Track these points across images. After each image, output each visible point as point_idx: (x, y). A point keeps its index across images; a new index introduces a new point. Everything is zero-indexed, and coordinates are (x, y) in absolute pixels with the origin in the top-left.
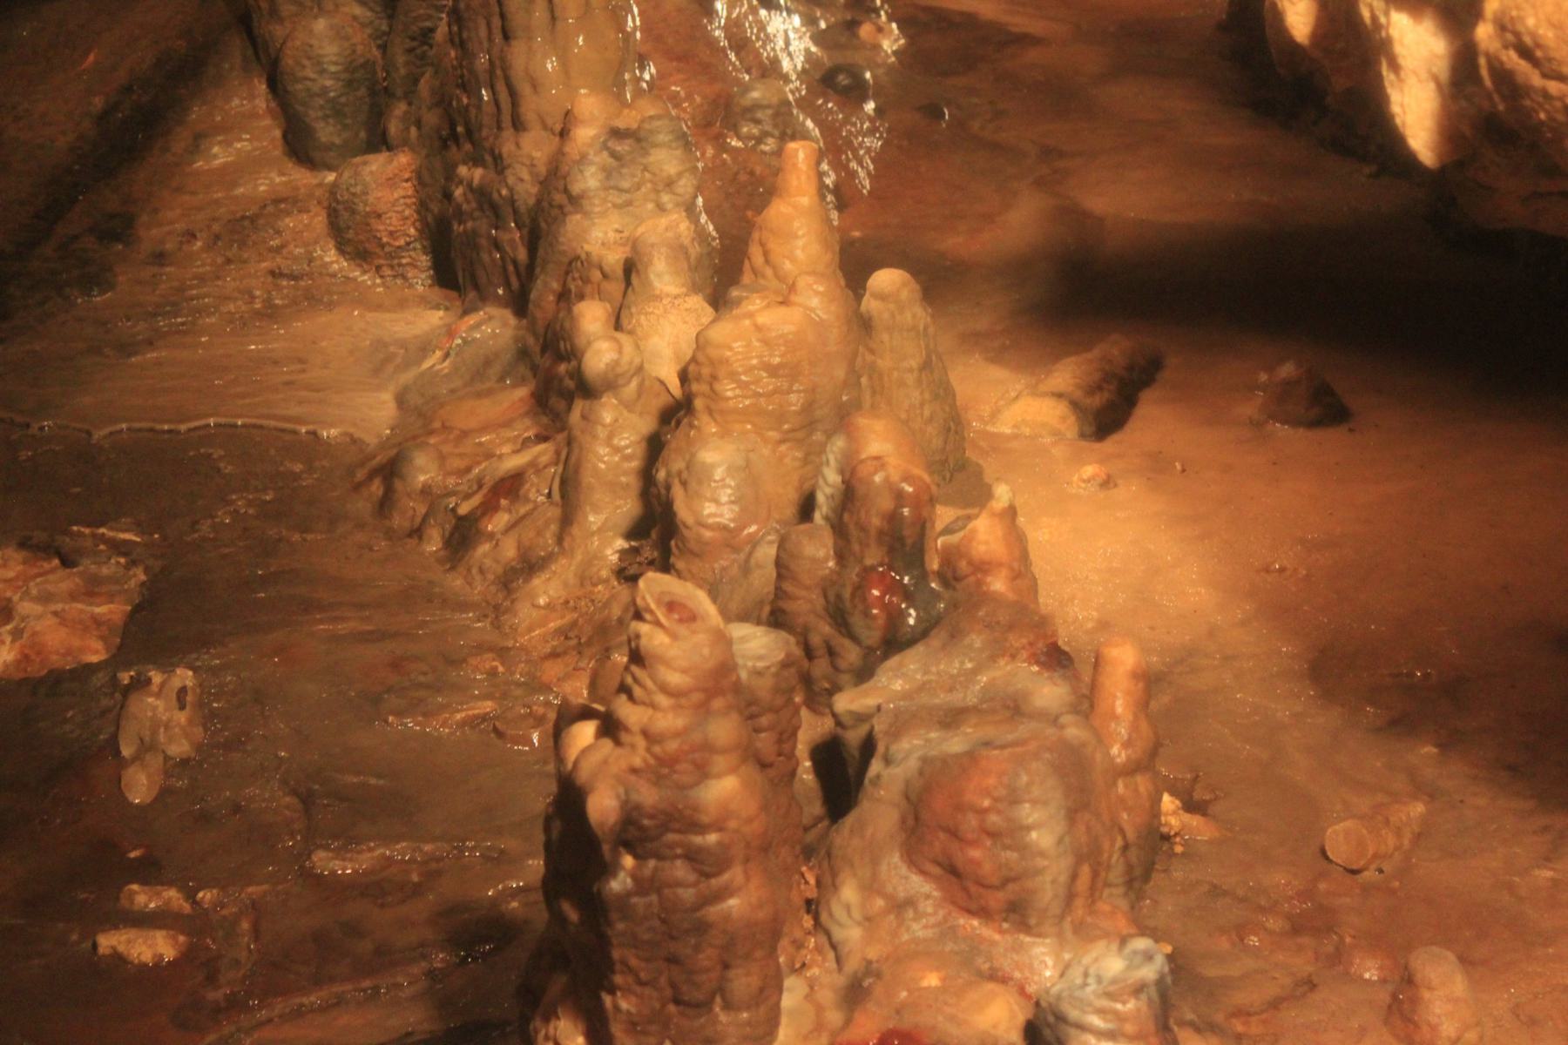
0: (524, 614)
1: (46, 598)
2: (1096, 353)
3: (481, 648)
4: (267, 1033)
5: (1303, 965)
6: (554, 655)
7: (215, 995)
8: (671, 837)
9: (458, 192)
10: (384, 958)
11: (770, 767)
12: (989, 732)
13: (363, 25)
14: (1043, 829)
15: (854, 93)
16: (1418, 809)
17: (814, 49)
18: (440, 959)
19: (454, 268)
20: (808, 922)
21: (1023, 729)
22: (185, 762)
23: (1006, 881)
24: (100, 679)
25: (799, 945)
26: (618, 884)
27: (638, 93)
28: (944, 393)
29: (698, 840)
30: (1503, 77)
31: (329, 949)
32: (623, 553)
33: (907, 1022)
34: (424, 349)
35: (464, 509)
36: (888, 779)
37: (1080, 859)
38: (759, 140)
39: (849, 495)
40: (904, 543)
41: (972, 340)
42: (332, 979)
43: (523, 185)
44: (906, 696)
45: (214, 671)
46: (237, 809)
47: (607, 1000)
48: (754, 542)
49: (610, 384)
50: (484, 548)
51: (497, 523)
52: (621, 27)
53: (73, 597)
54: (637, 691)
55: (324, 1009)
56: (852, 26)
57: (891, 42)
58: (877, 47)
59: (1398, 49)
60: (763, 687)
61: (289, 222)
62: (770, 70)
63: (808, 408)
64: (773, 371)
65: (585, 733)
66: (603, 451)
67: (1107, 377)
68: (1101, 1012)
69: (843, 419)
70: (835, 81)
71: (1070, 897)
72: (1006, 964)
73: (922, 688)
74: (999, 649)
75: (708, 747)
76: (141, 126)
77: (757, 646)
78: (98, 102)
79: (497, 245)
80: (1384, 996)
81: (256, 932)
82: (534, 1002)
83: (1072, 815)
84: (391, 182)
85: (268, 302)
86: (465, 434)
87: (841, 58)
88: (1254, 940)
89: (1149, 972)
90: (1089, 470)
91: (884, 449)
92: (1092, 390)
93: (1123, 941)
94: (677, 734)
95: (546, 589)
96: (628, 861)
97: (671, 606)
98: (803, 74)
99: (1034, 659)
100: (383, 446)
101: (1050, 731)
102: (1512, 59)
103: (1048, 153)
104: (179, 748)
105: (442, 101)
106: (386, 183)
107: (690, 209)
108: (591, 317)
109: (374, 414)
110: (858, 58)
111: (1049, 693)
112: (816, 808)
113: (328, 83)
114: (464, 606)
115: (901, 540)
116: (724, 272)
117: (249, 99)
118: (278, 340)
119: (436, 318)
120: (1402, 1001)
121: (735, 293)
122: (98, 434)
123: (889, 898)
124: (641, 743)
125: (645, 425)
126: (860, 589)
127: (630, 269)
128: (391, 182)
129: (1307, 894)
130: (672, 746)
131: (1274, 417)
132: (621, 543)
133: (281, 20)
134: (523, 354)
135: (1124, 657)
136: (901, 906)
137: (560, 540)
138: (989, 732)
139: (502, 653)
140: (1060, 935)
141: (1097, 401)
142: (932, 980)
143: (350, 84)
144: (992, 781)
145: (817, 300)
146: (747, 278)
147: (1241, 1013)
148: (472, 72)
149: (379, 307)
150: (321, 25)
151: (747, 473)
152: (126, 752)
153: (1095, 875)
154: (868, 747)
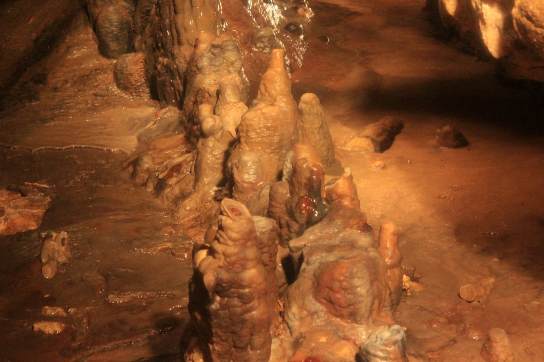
0: (182, 212)
1: (16, 207)
2: (380, 122)
3: (167, 225)
4: (93, 358)
5: (452, 334)
6: (192, 227)
7: (75, 345)
8: (233, 290)
9: (159, 67)
10: (133, 332)
11: (267, 266)
12: (343, 254)
13: (126, 9)
14: (362, 287)
15: (296, 32)
16: (492, 280)
17: (282, 17)
18: (153, 332)
19: (158, 93)
20: (280, 319)
21: (355, 253)
22: (64, 264)
23: (349, 305)
24: (34, 235)
25: (277, 327)
26: (214, 306)
27: (222, 32)
28: (327, 136)
29: (242, 291)
30: (522, 27)
31: (114, 329)
32: (216, 191)
33: (315, 354)
34: (147, 121)
35: (161, 176)
36: (308, 270)
37: (374, 298)
38: (263, 49)
39: (295, 171)
40: (314, 188)
41: (337, 118)
42: (115, 339)
43: (181, 64)
44: (315, 241)
45: (74, 233)
46: (82, 280)
47: (211, 346)
48: (262, 188)
49: (212, 133)
50: (168, 190)
51: (172, 181)
52: (215, 9)
53: (25, 207)
54: (221, 239)
55: (112, 349)
56: (296, 9)
57: (309, 14)
58: (304, 16)
59: (485, 17)
60: (265, 238)
61: (100, 77)
62: (267, 24)
63: (281, 141)
64: (268, 128)
65: (203, 254)
66: (209, 156)
67: (384, 131)
68: (382, 350)
69: (292, 145)
70: (290, 28)
71: (371, 311)
72: (349, 334)
73: (320, 238)
74: (347, 225)
75: (246, 259)
76: (49, 44)
77: (263, 224)
78: (34, 35)
79: (172, 85)
80: (480, 345)
81: (89, 323)
82: (185, 347)
83: (372, 282)
84: (136, 63)
85: (93, 105)
86: (161, 150)
87: (292, 20)
88: (435, 326)
89: (399, 337)
90: (378, 163)
91: (307, 156)
92: (379, 135)
93: (390, 326)
94: (235, 254)
95: (189, 204)
96: (218, 298)
97: (233, 210)
98: (279, 26)
99: (359, 228)
100: (133, 154)
101: (365, 253)
102: (524, 20)
103: (363, 53)
104: (62, 259)
105: (153, 35)
106: (134, 63)
107: (239, 72)
108: (205, 110)
109: (130, 143)
110: (298, 20)
111: (364, 240)
112: (283, 280)
113: (114, 29)
114: (161, 210)
115: (313, 187)
116: (251, 94)
117: (86, 34)
118: (96, 118)
119: (151, 110)
120: (487, 346)
121: (255, 101)
122: (34, 151)
123: (309, 311)
124: (222, 257)
125: (224, 147)
126: (298, 204)
127: (219, 93)
128: (136, 63)
129: (453, 310)
130: (233, 258)
131: (442, 144)
132: (215, 188)
133: (98, 7)
134: (181, 122)
135: (390, 228)
136: (313, 314)
137: (194, 187)
138: (343, 254)
139: (174, 226)
140: (368, 324)
141: (381, 139)
142: (323, 339)
143: (121, 29)
144: (344, 270)
145: (283, 104)
146: (259, 96)
147: (431, 351)
148: (164, 25)
149: (131, 106)
150: (111, 9)
151: (259, 164)
152: (44, 260)
153: (380, 303)
154: (301, 259)
